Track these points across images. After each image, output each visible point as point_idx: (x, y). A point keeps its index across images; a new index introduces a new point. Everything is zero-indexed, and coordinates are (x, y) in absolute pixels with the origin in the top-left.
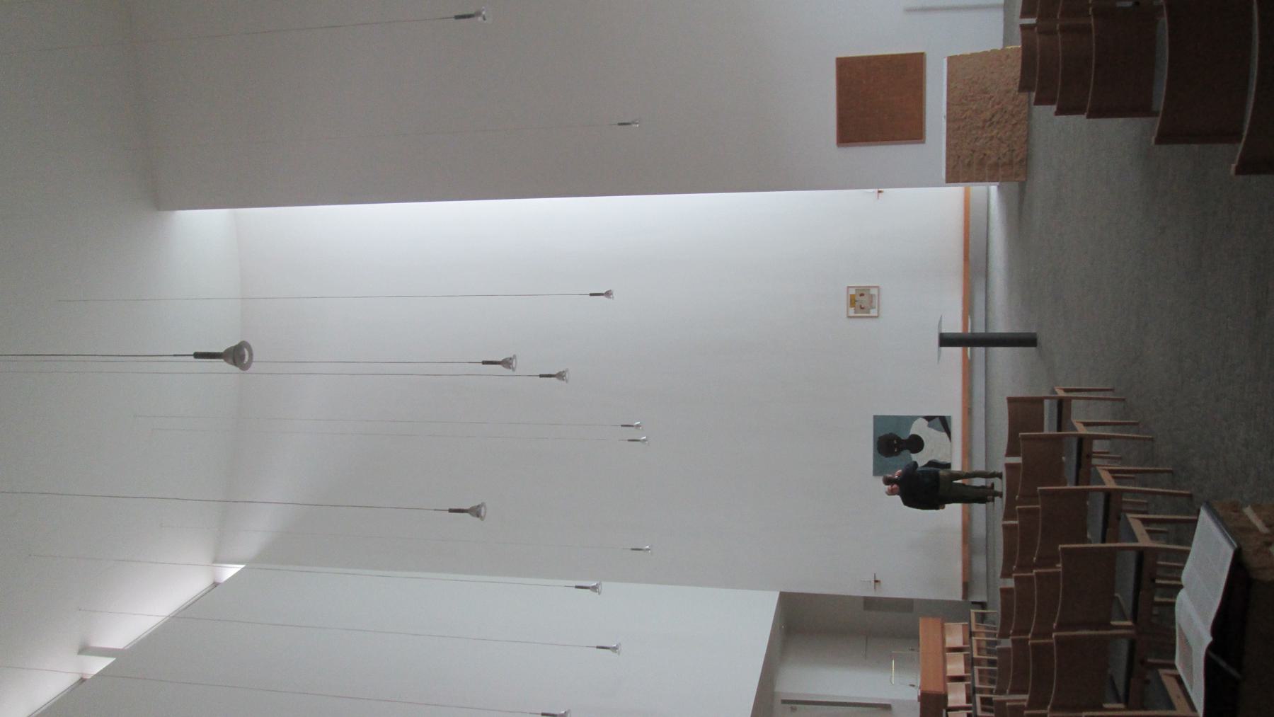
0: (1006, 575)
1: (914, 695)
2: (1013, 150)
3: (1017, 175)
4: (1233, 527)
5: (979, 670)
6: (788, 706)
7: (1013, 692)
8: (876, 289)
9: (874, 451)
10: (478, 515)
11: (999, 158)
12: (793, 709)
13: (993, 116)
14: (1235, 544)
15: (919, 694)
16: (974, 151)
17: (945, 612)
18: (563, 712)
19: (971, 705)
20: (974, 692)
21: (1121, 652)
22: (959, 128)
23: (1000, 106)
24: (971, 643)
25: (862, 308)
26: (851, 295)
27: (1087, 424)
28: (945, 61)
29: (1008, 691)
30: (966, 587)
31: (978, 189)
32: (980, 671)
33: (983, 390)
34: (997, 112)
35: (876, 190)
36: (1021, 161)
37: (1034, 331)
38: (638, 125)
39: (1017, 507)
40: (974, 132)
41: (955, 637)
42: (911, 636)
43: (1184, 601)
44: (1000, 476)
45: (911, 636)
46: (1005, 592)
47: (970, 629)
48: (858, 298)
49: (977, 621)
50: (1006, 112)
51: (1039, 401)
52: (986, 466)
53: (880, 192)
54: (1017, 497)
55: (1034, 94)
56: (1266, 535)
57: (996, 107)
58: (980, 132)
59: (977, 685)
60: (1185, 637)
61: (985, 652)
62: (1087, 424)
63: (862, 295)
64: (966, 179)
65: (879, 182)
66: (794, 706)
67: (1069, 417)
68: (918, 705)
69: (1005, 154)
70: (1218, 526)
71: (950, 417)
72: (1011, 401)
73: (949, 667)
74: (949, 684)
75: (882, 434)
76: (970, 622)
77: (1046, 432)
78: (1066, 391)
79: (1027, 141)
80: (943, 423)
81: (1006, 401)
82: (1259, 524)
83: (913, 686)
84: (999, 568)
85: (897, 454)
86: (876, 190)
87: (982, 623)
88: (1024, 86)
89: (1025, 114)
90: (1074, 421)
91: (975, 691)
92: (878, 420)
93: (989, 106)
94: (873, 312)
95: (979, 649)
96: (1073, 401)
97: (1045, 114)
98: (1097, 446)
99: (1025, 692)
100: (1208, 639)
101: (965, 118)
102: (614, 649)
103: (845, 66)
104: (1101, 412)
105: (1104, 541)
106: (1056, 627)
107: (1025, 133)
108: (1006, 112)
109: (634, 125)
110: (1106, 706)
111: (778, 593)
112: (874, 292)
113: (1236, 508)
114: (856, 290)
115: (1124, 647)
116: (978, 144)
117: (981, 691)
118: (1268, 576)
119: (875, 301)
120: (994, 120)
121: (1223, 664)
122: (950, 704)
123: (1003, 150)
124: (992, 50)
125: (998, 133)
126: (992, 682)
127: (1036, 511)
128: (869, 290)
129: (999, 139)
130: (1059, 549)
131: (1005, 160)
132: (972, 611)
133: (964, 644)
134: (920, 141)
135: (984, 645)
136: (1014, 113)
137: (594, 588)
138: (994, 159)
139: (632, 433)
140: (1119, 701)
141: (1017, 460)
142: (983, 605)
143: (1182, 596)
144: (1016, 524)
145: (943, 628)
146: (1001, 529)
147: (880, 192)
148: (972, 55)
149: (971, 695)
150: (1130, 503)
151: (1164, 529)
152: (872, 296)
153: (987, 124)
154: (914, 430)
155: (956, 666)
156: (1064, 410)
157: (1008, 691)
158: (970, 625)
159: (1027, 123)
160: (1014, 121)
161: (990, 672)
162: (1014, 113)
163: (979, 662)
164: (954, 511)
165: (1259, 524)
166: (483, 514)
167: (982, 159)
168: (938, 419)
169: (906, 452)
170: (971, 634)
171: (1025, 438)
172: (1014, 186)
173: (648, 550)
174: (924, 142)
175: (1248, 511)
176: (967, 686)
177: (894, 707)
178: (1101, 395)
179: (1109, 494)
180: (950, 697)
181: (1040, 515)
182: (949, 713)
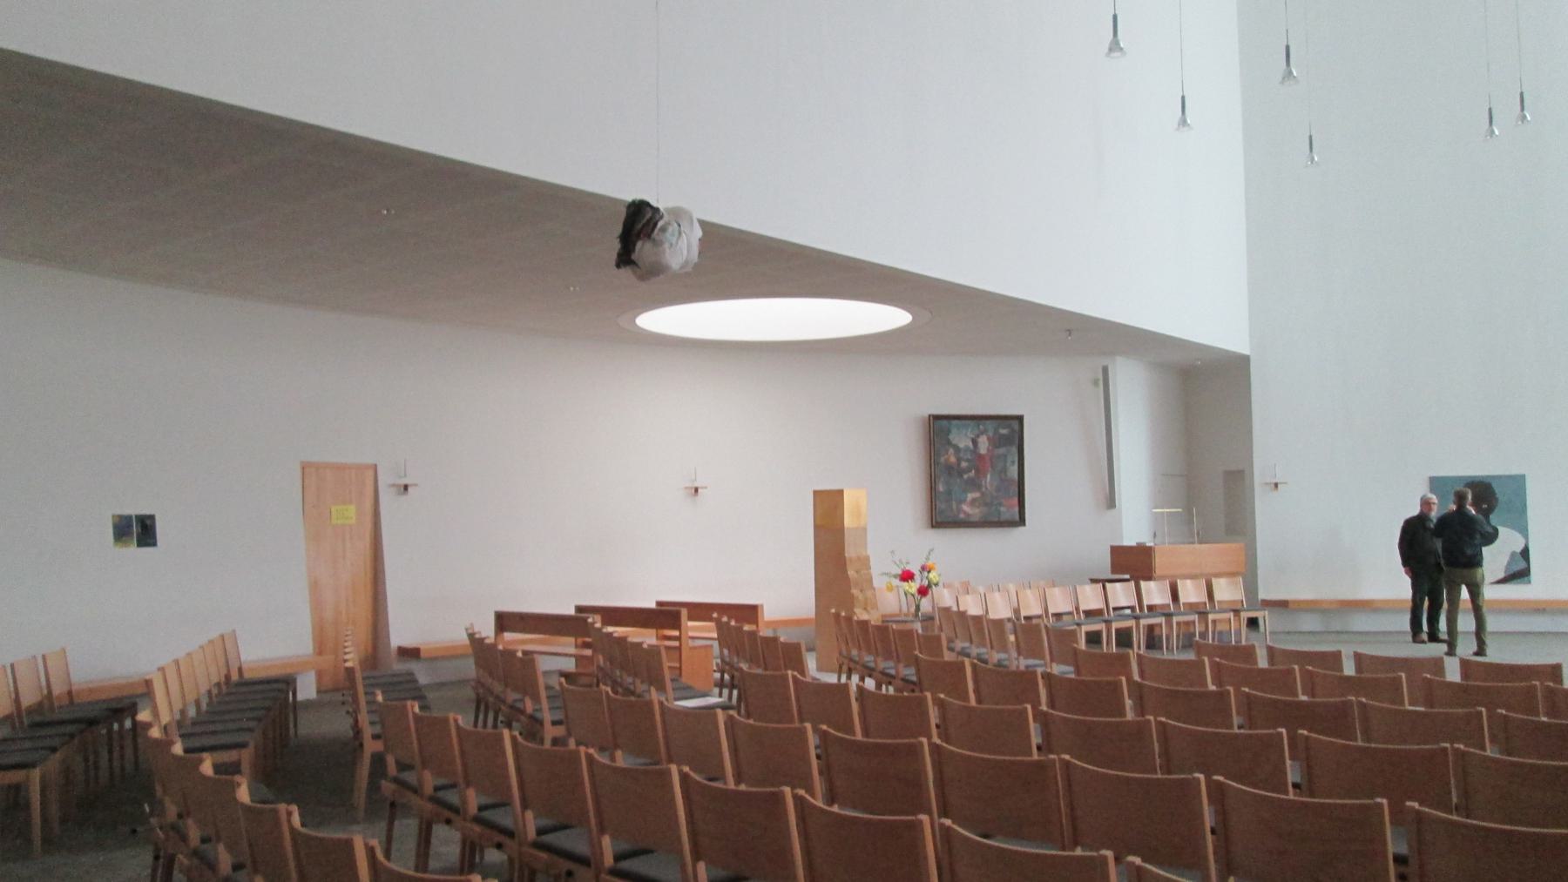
0: (1358, 657)
6: (1101, 377)
9: (1470, 477)
12: (1096, 383)
18: (1122, 45)
33: (1367, 628)
39: (1403, 675)
41: (1226, 591)
44: (1481, 651)
52: (1464, 633)
59: (1175, 619)
66: (1101, 383)
73: (1188, 582)
74: (1167, 583)
75: (1494, 485)
84: (1368, 650)
91: (1169, 616)
92: (1518, 482)
96: (536, 656)
102: (1183, 122)
111: (1245, 351)
117: (1169, 624)
122: (1143, 584)
133: (1219, 602)
155: (1191, 592)
164: (1400, 586)
170: (1236, 612)
177: (1113, 512)
180: (1152, 584)
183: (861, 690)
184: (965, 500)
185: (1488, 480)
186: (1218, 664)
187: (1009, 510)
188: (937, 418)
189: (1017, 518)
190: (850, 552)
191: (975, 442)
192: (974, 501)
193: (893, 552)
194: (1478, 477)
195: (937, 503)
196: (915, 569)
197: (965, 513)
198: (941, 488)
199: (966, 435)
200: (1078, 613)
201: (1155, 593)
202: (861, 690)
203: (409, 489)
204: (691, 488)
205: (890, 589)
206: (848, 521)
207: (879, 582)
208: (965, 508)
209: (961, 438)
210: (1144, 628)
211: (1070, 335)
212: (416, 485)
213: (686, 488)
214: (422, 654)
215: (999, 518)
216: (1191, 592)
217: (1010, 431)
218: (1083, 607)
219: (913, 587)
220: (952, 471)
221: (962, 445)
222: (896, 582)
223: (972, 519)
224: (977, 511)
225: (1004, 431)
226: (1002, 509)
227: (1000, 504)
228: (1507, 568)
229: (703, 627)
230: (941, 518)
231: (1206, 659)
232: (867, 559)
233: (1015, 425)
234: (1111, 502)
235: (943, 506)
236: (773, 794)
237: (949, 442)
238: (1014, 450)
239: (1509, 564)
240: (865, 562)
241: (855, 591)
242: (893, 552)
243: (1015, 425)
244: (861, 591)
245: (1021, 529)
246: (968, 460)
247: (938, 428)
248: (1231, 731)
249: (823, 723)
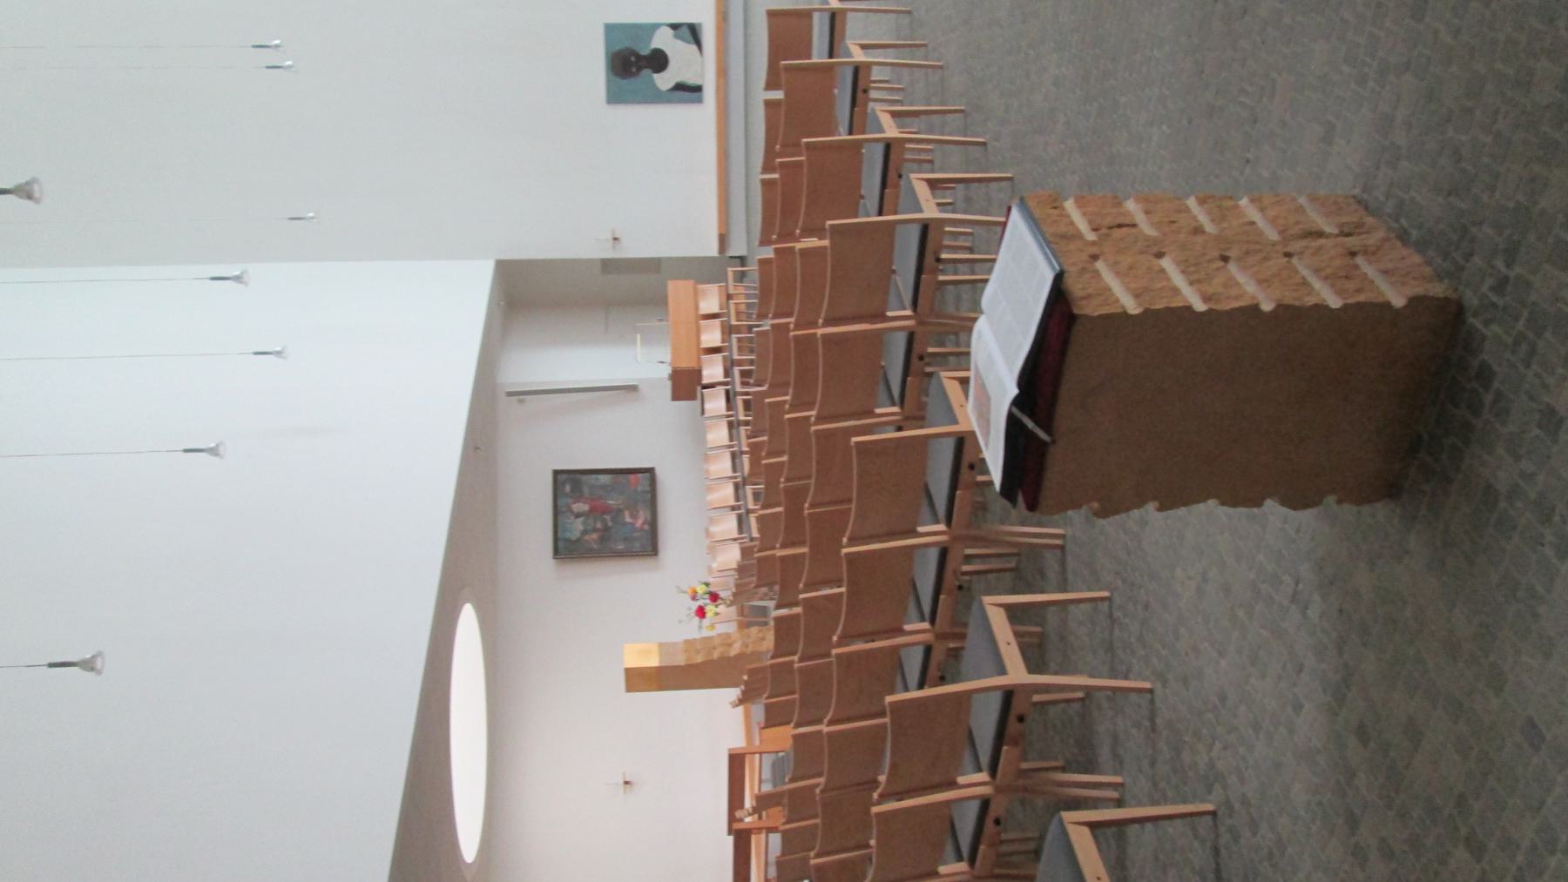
1: (666, 371)
4: (1054, 239)
5: (739, 338)
6: (515, 398)
7: (784, 546)
10: (30, 197)
12: (521, 401)
14: (1057, 268)
17: (700, 270)
19: (729, 379)
21: (899, 344)
24: (728, 307)
27: (864, 47)
29: (770, 315)
30: (723, 240)
32: (739, 340)
41: (710, 303)
42: (658, 301)
43: (983, 329)
45: (658, 301)
46: (769, 104)
51: (806, 15)
60: (982, 380)
61: (743, 317)
62: (864, 47)
67: (843, 37)
68: (669, 384)
70: (1035, 237)
74: (705, 357)
75: (617, 48)
77: (815, 60)
82: (1082, 225)
83: (662, 362)
87: (741, 282)
92: (610, 29)
95: (738, 313)
98: (876, 74)
99: (802, 543)
100: (1013, 391)
104: (881, 30)
105: (880, 213)
106: (823, 324)
113: (1055, 202)
115: (900, 341)
121: (1030, 424)
126: (752, 351)
132: (730, 269)
133: (721, 309)
135: (743, 308)
137: (238, 279)
139: (269, 57)
141: (778, 95)
142: (742, 260)
143: (982, 326)
145: (696, 292)
150: (913, 149)
151: (930, 147)
155: (712, 336)
156: (837, 27)
161: (750, 340)
163: (737, 329)
165: (1082, 225)
166: (37, 195)
169: (646, 72)
170: (729, 297)
171: (788, 69)
173: (313, 218)
176: (724, 357)
179: (888, 146)
180: (705, 373)
181: (805, 170)
183: (784, 483)
184: (633, 524)
186: (806, 585)
187: (642, 481)
188: (556, 552)
189: (647, 475)
190: (680, 660)
191: (578, 516)
192: (634, 516)
193: (680, 622)
195: (635, 550)
196: (695, 605)
197: (644, 523)
198: (621, 547)
199: (571, 523)
200: (739, 508)
201: (713, 371)
202: (784, 483)
203: (617, 236)
204: (625, 789)
205: (712, 626)
206: (653, 662)
207: (706, 633)
208: (639, 523)
209: (576, 527)
212: (624, 774)
213: (625, 793)
215: (647, 492)
216: (712, 336)
217: (567, 482)
219: (711, 609)
220: (605, 535)
221: (581, 528)
222: (706, 622)
223: (649, 518)
224: (641, 513)
225: (568, 488)
227: (636, 491)
228: (688, 42)
229: (756, 844)
230: (648, 546)
231: (802, 596)
232: (687, 642)
233: (562, 477)
234: (632, 389)
235: (637, 545)
236: (859, 453)
237: (578, 540)
238: (584, 478)
239: (683, 39)
240: (689, 643)
241: (716, 655)
242: (680, 622)
243: (562, 477)
244: (714, 648)
245: (658, 472)
246: (595, 522)
247: (566, 549)
248: (889, 726)
249: (831, 638)
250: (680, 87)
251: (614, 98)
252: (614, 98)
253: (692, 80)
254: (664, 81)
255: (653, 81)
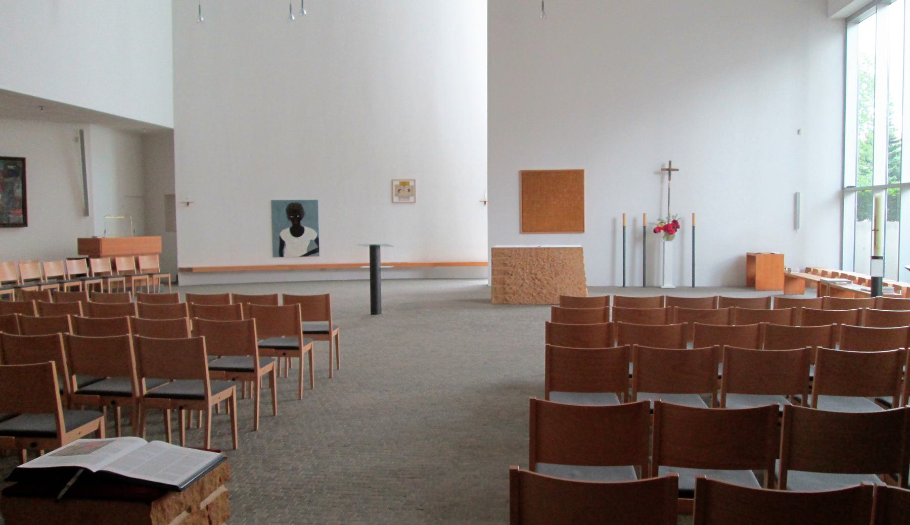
0: (189, 297)
1: (99, 234)
2: (514, 295)
3: (496, 298)
4: (199, 483)
6: (79, 135)
8: (413, 201)
9: (291, 201)
11: (508, 285)
12: (76, 139)
13: (539, 280)
14: (182, 487)
15: (98, 237)
16: (514, 267)
17: (168, 256)
20: (103, 278)
21: (121, 387)
22: (532, 256)
23: (546, 284)
24: (145, 274)
25: (399, 190)
26: (408, 183)
28: (580, 246)
29: (140, 302)
30: (189, 270)
31: (487, 271)
32: (121, 282)
34: (541, 282)
35: (486, 200)
36: (506, 300)
37: (382, 312)
38: (541, 17)
40: (528, 267)
41: (147, 263)
45: (147, 230)
47: (156, 274)
48: (407, 188)
49: (161, 278)
50: (542, 288)
51: (327, 317)
53: (485, 202)
54: (250, 303)
55: (559, 306)
56: (198, 508)
57: (545, 282)
58: (528, 271)
59: (110, 280)
61: (138, 285)
63: (409, 190)
64: (494, 262)
65: (492, 202)
68: (90, 236)
69: (511, 289)
71: (318, 255)
72: (327, 297)
75: (304, 207)
76: (161, 273)
77: (302, 323)
78: (336, 337)
79: (520, 304)
80: (314, 251)
81: (326, 293)
82: (209, 499)
85: (289, 218)
86: (486, 200)
88: (564, 300)
89: (540, 302)
90: (312, 343)
92: (315, 203)
93: (546, 277)
94: (396, 199)
95: (140, 281)
96: (898, 222)
97: (546, 314)
98: (294, 360)
101: (538, 261)
103: (578, 175)
104: (320, 362)
107: (526, 302)
108: (542, 288)
109: (542, 14)
110: (74, 377)
112: (412, 199)
113: (224, 480)
114: (413, 186)
116: (519, 270)
117: (105, 283)
118: (155, 515)
119: (406, 200)
120: (536, 280)
122: (92, 260)
123: (514, 287)
124: (585, 278)
125: (526, 284)
126: (114, 290)
127: (239, 317)
128: (413, 196)
129: (522, 285)
130: (201, 336)
131: (507, 289)
133: (143, 270)
134: (522, 229)
135: (143, 284)
136: (541, 294)
138: (508, 281)
140: (79, 387)
141: (280, 303)
142: (175, 283)
144: (229, 303)
145: (154, 254)
146: (226, 293)
147: (485, 202)
148: (583, 265)
149: (102, 276)
152: (408, 197)
153: (533, 276)
154: (307, 230)
155: (124, 264)
156: (315, 336)
157: (140, 302)
158: (158, 273)
159: (534, 303)
160: (535, 294)
161: (121, 290)
162: (541, 294)
167: (509, 274)
168: (316, 247)
169: (290, 224)
170: (151, 275)
171: (296, 308)
172: (488, 296)
174: (520, 233)
175: (222, 489)
176: (109, 273)
177: (87, 218)
178: (334, 361)
180: (98, 260)
182: (85, 260)
185: (300, 203)
187: (16, 217)
189: (22, 221)
194: (296, 201)
201: (99, 265)
203: (190, 204)
210: (87, 285)
211: (42, 109)
214: (105, 288)
216: (124, 264)
218: (47, 275)
225: (12, 167)
226: (11, 216)
227: (9, 213)
234: (86, 213)
238: (19, 179)
245: (25, 228)
250: (282, 244)
251: (275, 205)
252: (275, 205)
253: (287, 250)
254: (286, 234)
255: (288, 227)
